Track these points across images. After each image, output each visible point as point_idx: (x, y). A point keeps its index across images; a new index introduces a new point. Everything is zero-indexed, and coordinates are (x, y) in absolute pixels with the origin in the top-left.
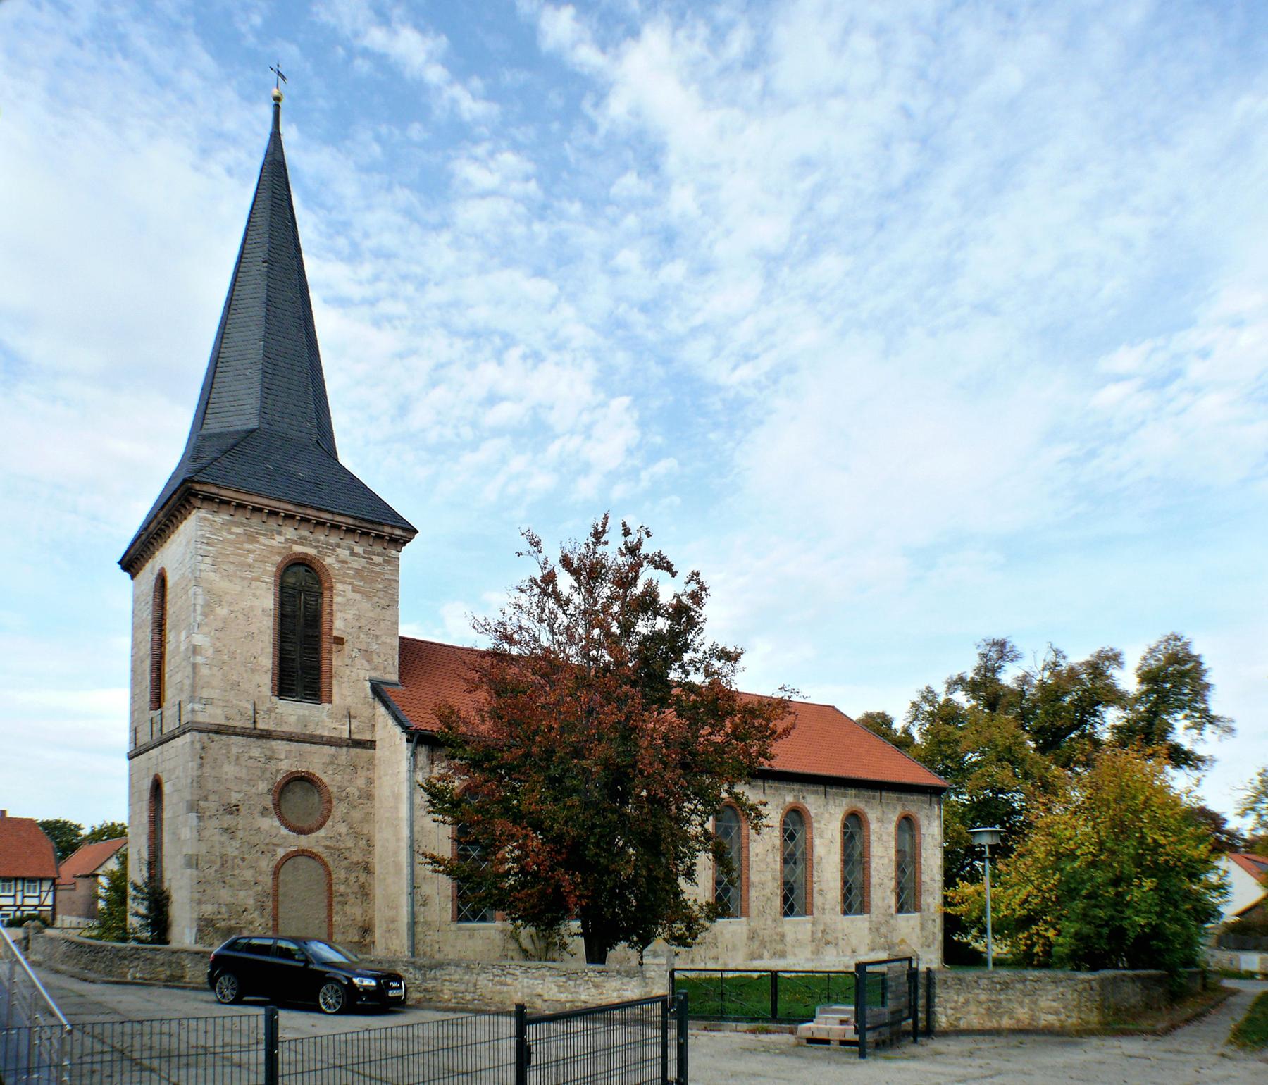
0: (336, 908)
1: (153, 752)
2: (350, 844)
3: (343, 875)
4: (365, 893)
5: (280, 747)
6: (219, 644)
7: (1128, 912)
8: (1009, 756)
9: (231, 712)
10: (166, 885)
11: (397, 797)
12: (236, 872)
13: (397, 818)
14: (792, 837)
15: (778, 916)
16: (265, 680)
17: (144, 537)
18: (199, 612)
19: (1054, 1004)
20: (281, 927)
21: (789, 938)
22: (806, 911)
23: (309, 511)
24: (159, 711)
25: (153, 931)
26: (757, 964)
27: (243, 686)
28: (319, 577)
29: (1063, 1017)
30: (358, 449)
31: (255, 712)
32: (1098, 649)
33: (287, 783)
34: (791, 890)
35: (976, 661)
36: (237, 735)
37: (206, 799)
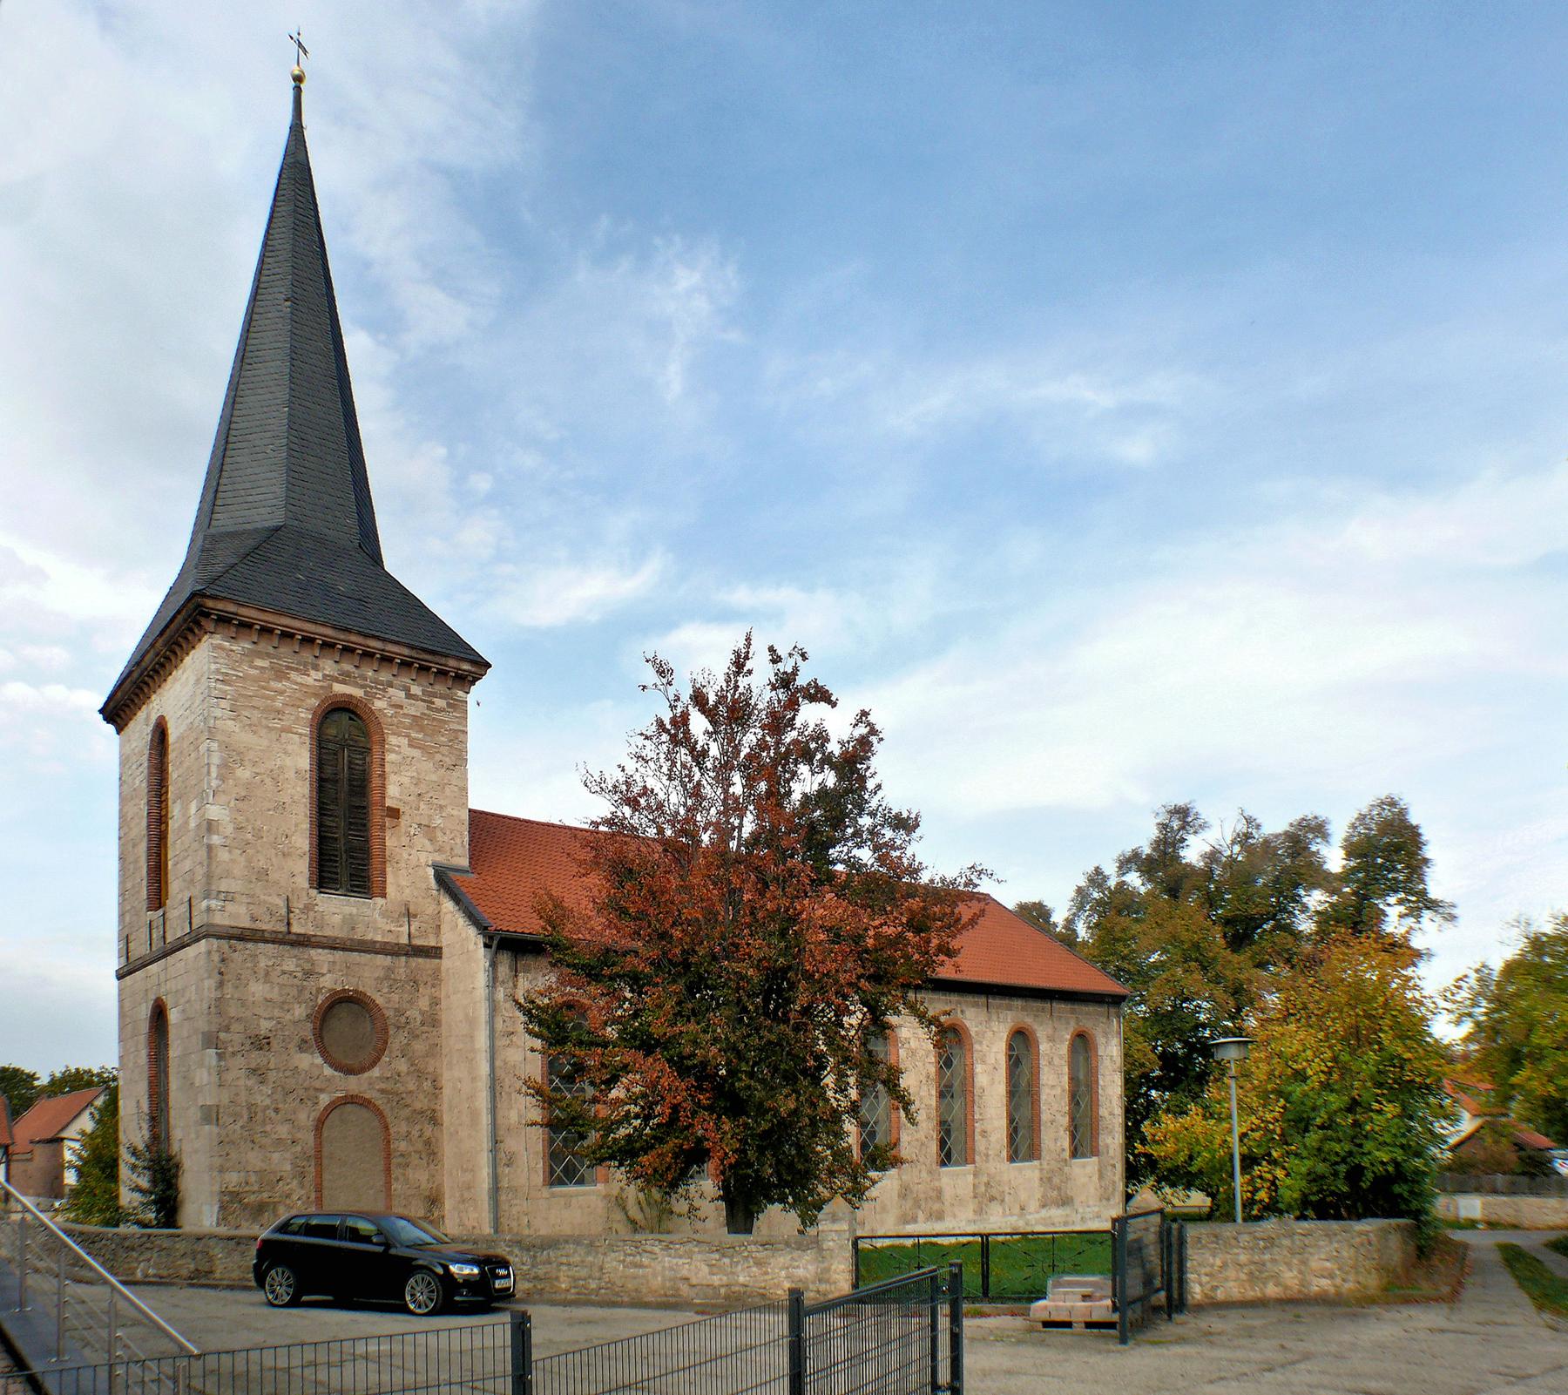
0: (396, 1172)
1: (153, 968)
2: (411, 1086)
3: (403, 1128)
4: (431, 1152)
5: (321, 956)
6: (240, 819)
7: (1368, 1146)
8: (1196, 957)
9: (259, 911)
10: (175, 1148)
11: (471, 1022)
12: (268, 1128)
13: (473, 1050)
14: (948, 1063)
15: (934, 1166)
16: (300, 868)
17: (135, 675)
18: (214, 775)
19: (1328, 1264)
20: (326, 1202)
21: (948, 1194)
22: (968, 1159)
23: (353, 638)
24: (160, 912)
25: (158, 1212)
26: (910, 1229)
27: (273, 876)
28: (366, 725)
29: (1338, 1281)
30: (408, 557)
31: (289, 911)
32: (1299, 816)
33: (331, 1007)
34: (948, 1132)
35: (1154, 833)
36: (266, 941)
37: (227, 1029)
